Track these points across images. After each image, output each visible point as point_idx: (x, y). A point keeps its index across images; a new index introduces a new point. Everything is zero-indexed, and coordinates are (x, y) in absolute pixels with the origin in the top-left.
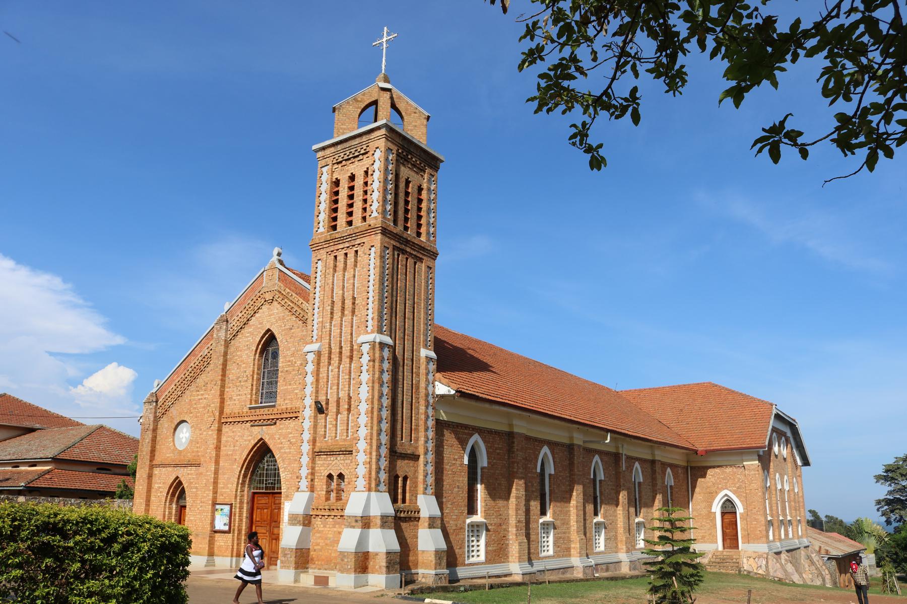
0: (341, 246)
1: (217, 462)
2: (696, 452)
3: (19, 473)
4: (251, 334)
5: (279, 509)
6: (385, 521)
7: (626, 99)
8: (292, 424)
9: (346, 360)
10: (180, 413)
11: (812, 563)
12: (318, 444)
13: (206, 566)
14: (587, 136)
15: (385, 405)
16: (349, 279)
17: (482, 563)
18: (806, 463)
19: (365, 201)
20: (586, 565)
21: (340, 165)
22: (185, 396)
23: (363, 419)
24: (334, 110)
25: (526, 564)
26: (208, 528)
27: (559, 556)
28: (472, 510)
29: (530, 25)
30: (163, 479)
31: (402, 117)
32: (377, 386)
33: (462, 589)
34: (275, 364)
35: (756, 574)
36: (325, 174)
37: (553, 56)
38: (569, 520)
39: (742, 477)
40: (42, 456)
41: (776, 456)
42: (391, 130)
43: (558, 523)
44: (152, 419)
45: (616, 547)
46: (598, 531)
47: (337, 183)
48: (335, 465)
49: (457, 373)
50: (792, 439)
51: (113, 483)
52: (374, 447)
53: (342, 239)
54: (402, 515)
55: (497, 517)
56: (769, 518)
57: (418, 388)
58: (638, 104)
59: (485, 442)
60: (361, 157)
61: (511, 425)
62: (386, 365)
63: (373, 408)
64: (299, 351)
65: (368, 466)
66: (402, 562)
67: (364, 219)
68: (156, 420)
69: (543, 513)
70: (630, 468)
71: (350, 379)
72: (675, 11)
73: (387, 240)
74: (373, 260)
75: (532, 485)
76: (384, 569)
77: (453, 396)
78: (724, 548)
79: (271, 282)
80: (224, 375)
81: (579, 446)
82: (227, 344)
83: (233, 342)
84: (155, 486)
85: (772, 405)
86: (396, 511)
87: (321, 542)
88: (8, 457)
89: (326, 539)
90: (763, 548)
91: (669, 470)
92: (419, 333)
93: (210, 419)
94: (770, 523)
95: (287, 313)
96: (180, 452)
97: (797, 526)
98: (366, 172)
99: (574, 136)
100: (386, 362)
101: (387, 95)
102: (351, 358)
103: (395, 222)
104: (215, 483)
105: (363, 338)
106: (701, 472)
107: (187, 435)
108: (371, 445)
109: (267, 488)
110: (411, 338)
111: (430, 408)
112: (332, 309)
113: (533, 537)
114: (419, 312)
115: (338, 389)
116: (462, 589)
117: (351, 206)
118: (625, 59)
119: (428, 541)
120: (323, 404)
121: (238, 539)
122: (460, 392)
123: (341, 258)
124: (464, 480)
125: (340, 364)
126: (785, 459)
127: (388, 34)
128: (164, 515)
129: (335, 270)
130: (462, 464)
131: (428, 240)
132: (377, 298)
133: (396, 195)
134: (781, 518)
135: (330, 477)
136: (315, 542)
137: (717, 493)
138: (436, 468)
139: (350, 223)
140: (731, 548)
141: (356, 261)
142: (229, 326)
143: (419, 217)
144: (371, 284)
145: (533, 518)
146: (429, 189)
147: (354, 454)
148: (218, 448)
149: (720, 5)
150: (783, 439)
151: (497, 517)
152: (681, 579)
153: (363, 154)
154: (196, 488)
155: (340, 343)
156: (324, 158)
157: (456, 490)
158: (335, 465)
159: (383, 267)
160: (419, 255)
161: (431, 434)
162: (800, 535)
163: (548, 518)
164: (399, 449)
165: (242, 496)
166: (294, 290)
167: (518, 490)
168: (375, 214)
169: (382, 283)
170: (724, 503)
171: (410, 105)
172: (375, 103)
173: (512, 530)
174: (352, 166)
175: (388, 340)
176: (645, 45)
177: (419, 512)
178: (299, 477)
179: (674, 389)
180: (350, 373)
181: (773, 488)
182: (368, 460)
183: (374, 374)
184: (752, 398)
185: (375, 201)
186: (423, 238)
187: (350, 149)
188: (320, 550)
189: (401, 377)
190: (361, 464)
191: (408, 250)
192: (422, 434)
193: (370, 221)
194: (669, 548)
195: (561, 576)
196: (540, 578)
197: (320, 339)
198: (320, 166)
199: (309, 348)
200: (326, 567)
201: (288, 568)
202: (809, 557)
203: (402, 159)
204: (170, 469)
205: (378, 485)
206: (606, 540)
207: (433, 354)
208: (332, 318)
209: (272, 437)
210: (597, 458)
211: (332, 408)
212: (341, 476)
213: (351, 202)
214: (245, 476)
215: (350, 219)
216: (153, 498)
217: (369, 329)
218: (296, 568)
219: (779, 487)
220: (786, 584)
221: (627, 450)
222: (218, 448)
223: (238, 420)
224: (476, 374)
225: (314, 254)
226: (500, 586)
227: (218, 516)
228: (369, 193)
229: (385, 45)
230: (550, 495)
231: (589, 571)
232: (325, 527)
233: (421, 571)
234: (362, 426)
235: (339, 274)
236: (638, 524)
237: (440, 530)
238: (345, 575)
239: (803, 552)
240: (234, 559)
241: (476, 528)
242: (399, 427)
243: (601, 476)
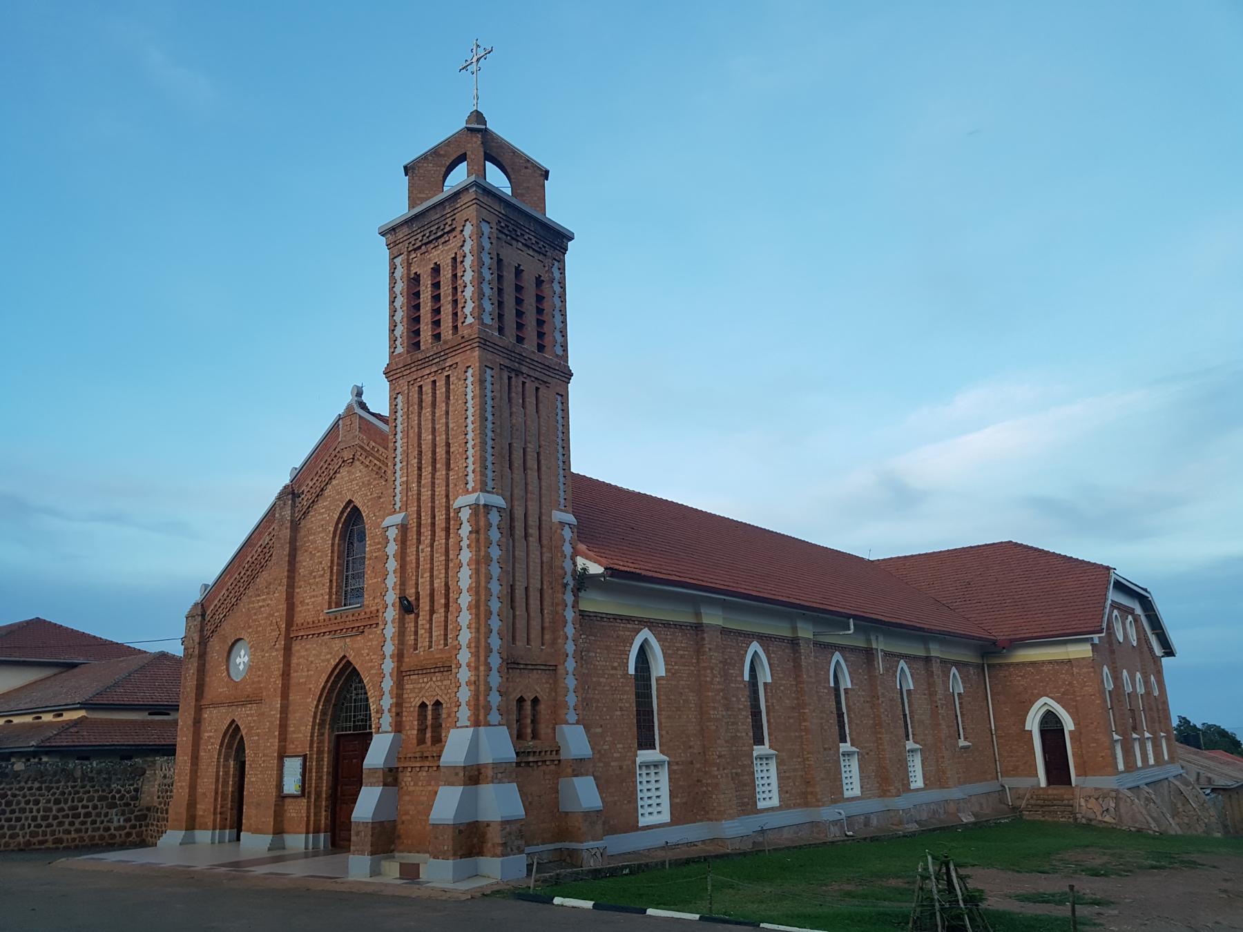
1: (285, 695)
4: (327, 508)
26: (274, 792)
27: (788, 807)
30: (216, 722)
40: (69, 701)
47: (416, 279)
65: (473, 688)
67: (455, 328)
70: (891, 670)
73: (490, 356)
74: (470, 387)
75: (739, 700)
78: (1049, 782)
83: (303, 522)
102: (447, 530)
107: (246, 659)
112: (420, 462)
120: (412, 599)
123: (427, 389)
139: (437, 337)
141: (448, 391)
144: (469, 421)
147: (454, 671)
150: (1130, 618)
154: (258, 735)
168: (470, 320)
175: (499, 501)
177: (557, 752)
182: (473, 679)
190: (463, 684)
197: (406, 506)
204: (223, 710)
207: (570, 518)
211: (425, 605)
222: (286, 674)
223: (316, 631)
240: (311, 836)
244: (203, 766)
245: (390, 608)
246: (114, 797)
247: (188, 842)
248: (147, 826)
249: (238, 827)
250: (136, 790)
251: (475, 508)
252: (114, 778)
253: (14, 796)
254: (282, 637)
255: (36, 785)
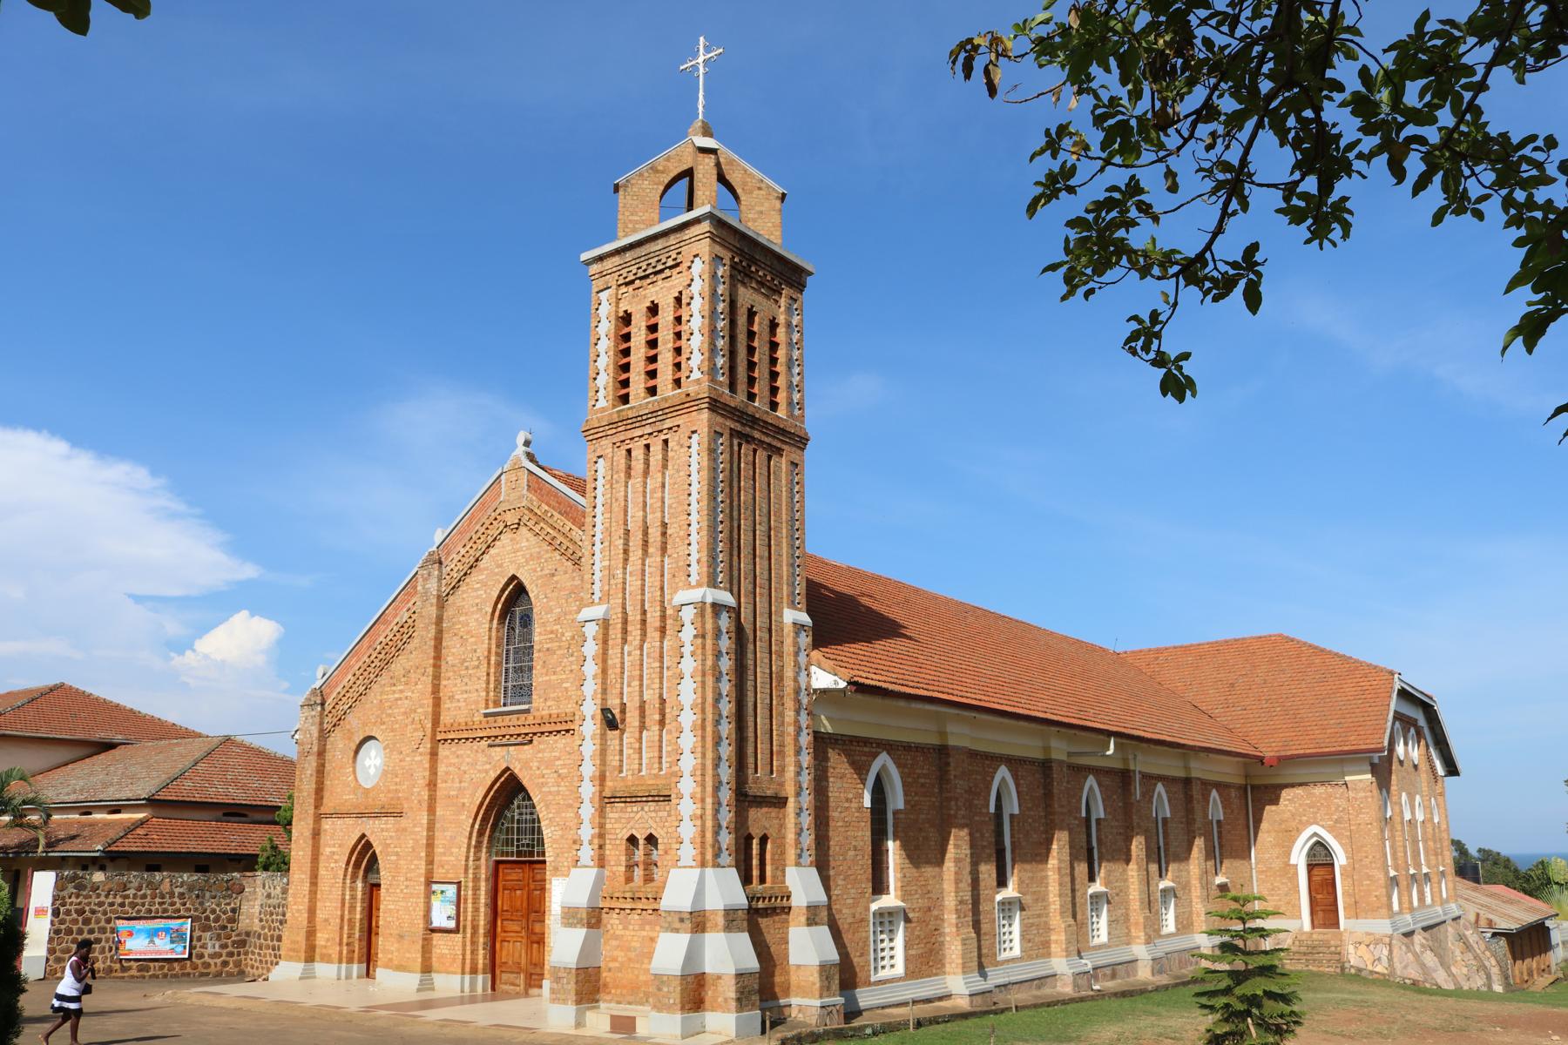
0: (638, 432)
1: (431, 810)
2: (1261, 760)
3: (93, 824)
5: (543, 889)
6: (731, 919)
7: (1234, 265)
8: (561, 742)
9: (653, 634)
10: (365, 724)
11: (1468, 947)
12: (609, 783)
13: (419, 990)
14: (1158, 335)
15: (725, 714)
16: (653, 491)
17: (900, 979)
18: (1452, 770)
19: (678, 351)
20: (1077, 970)
21: (631, 288)
22: (371, 694)
23: (688, 741)
24: (616, 188)
25: (975, 976)
27: (1030, 958)
28: (879, 887)
29: (1053, 132)
30: (339, 838)
31: (737, 197)
32: (710, 681)
33: (868, 1031)
34: (527, 637)
35: (1372, 972)
36: (605, 304)
37: (1096, 182)
38: (1047, 893)
39: (1343, 803)
40: (130, 795)
41: (1401, 763)
42: (719, 223)
43: (1027, 900)
44: (316, 734)
45: (1128, 934)
46: (1096, 910)
47: (626, 319)
48: (642, 820)
49: (846, 647)
50: (1426, 731)
51: (249, 838)
52: (709, 789)
53: (639, 420)
54: (761, 905)
55: (922, 896)
56: (1392, 873)
57: (781, 679)
58: (1259, 275)
59: (899, 765)
60: (668, 273)
61: (943, 734)
62: (726, 643)
63: (704, 720)
64: (569, 618)
65: (699, 823)
66: (762, 990)
68: (323, 735)
69: (1002, 883)
70: (1148, 794)
71: (662, 668)
72: (1335, 95)
73: (719, 419)
75: (982, 835)
76: (733, 1004)
77: (843, 691)
78: (1313, 927)
79: (514, 493)
80: (438, 657)
81: (1061, 762)
82: (442, 602)
83: (451, 598)
84: (326, 851)
85: (1392, 673)
86: (750, 899)
87: (620, 954)
88: (73, 798)
89: (629, 949)
90: (1382, 926)
91: (1214, 793)
92: (779, 583)
93: (417, 735)
94: (1394, 881)
95: (545, 546)
96: (366, 791)
97: (1440, 883)
98: (678, 300)
99: (1134, 337)
100: (725, 637)
101: (709, 161)
102: (663, 630)
103: (732, 387)
104: (430, 845)
105: (682, 596)
106: (1271, 794)
107: (378, 762)
108: (703, 786)
109: (519, 854)
110: (766, 591)
111: (804, 714)
112: (626, 544)
113: (985, 927)
114: (779, 545)
115: (641, 685)
116: (868, 1031)
117: (653, 359)
118: (1234, 185)
119: (806, 948)
120: (616, 712)
121: (473, 943)
122: (855, 683)
123: (638, 453)
124: (865, 834)
125: (643, 641)
126: (1416, 767)
127: (708, 49)
128: (343, 900)
129: (628, 476)
130: (860, 808)
131: (791, 415)
132: (705, 524)
133: (733, 338)
134: (1412, 871)
135: (632, 840)
136: (610, 956)
137: (1299, 831)
138: (817, 818)
139: (652, 391)
140: (1325, 926)
141: (665, 459)
142: (445, 571)
143: (774, 375)
144: (693, 499)
145: (984, 893)
146: (789, 325)
147: (674, 801)
148: (432, 785)
149: (1425, 81)
150: (1412, 730)
151: (922, 896)
152: (1262, 1024)
153: (671, 268)
154: (397, 854)
155: (643, 605)
156: (602, 275)
157: (852, 853)
158: (642, 820)
159: (713, 470)
160: (775, 443)
161: (806, 759)
162: (1448, 898)
163: (1011, 891)
164: (752, 789)
165: (477, 868)
166: (557, 503)
167: (958, 846)
168: (696, 375)
169: (713, 497)
170: (1312, 848)
171: (751, 175)
172: (689, 173)
173: (950, 918)
174: (652, 289)
175: (727, 598)
176: (1273, 159)
177: (788, 897)
178: (577, 842)
179: (1219, 647)
180: (662, 657)
181: (1397, 819)
182: (699, 812)
183: (704, 660)
184: (1356, 661)
185: (696, 352)
186: (781, 413)
187: (647, 258)
188: (619, 970)
189: (750, 662)
191: (757, 435)
192: (790, 760)
193: (689, 387)
194: (1239, 965)
195: (1038, 993)
196: (1002, 999)
197: (606, 597)
198: (595, 290)
199: (587, 613)
200: (631, 998)
201: (565, 1001)
202: (1461, 938)
203: (740, 274)
204: (349, 821)
205: (717, 855)
206: (1110, 923)
207: (805, 618)
208: (626, 560)
209: (526, 765)
210: (1091, 781)
211: (632, 719)
212: (651, 840)
213: (652, 352)
214: (481, 833)
215: (651, 383)
216: (322, 872)
217: (693, 579)
218: (579, 1002)
219: (1408, 816)
220: (1425, 991)
221: (1142, 764)
222: (432, 785)
223: (466, 736)
224: (879, 645)
225: (590, 447)
226: (934, 1021)
227: (436, 903)
228: (684, 337)
229: (701, 71)
230: (1013, 851)
231: (1082, 981)
232: (625, 928)
233: (795, 1001)
234: (687, 752)
235: (636, 481)
236: (1165, 891)
237: (826, 928)
238: (664, 1015)
239: (1450, 929)
240: (467, 977)
241: (886, 919)
242: (750, 750)
243: (1099, 811)
244: (323, 886)
245: (589, 720)
246: (207, 918)
247: (307, 976)
248: (246, 953)
249: (368, 959)
250: (234, 910)
251: (701, 606)
252: (208, 894)
253: (93, 912)
254: (427, 740)
255: (119, 900)
